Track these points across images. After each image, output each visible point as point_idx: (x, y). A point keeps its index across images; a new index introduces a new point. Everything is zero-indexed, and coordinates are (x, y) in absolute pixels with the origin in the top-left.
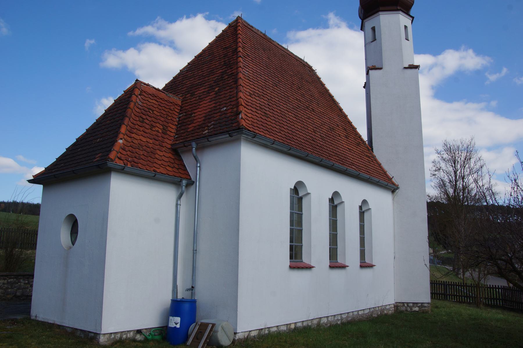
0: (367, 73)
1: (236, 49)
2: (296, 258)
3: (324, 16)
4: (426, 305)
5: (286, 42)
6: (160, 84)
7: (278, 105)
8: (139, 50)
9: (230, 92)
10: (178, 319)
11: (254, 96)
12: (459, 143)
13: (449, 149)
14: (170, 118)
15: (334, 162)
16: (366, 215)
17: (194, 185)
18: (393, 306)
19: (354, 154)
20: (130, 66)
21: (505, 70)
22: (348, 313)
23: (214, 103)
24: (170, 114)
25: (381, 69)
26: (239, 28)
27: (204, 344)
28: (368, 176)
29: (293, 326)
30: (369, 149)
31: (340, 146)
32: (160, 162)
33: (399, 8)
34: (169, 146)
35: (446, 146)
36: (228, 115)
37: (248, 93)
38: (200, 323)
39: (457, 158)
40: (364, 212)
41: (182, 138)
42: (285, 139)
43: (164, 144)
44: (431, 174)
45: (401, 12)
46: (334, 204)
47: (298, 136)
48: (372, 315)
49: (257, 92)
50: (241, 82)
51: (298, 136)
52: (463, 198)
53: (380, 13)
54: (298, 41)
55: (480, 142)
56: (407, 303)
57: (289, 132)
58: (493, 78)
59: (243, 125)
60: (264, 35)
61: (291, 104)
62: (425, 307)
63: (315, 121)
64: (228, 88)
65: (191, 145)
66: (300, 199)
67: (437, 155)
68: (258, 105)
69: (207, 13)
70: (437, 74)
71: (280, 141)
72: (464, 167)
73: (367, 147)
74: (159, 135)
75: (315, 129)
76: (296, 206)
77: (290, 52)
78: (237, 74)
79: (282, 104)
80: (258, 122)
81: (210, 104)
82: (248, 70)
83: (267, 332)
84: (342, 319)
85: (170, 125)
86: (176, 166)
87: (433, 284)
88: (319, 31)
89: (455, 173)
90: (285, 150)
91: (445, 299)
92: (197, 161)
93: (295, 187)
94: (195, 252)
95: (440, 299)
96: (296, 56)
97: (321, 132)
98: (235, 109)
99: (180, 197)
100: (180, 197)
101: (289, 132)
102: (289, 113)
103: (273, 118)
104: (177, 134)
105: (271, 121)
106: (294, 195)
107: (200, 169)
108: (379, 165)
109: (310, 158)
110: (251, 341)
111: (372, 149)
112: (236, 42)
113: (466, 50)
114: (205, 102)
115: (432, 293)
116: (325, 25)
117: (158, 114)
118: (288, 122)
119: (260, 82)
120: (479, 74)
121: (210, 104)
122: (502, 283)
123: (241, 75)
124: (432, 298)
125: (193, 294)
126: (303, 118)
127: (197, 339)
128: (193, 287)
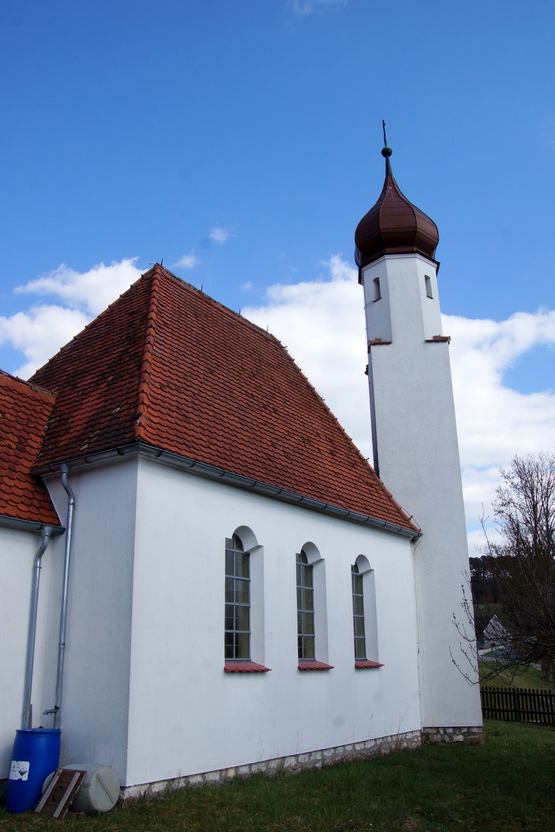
0: (369, 351)
1: (147, 315)
3: (324, 263)
4: (475, 730)
5: (261, 302)
6: (26, 373)
7: (211, 403)
8: (33, 317)
9: (129, 383)
10: (25, 766)
11: (168, 389)
14: (32, 425)
15: (304, 494)
17: (65, 534)
19: (343, 481)
20: (18, 341)
22: (335, 748)
23: (104, 401)
24: (33, 419)
25: (389, 343)
26: (156, 282)
27: (64, 808)
28: (365, 517)
29: (231, 773)
31: (319, 468)
32: (7, 497)
33: (415, 249)
34: (27, 471)
36: (121, 420)
37: (157, 385)
38: (61, 771)
39: (536, 483)
40: (361, 576)
41: (49, 457)
43: (18, 468)
44: (495, 511)
45: (418, 255)
46: (307, 564)
47: (242, 452)
48: (379, 751)
49: (176, 382)
50: (146, 367)
51: (242, 452)
53: (386, 257)
54: (284, 302)
57: (225, 446)
59: (139, 435)
60: (200, 292)
61: (235, 401)
62: (474, 734)
64: (128, 376)
65: (60, 469)
66: (246, 556)
67: (503, 480)
68: (174, 403)
69: (136, 258)
70: (505, 352)
74: (12, 452)
75: (274, 441)
77: (243, 319)
78: (143, 355)
79: (218, 401)
80: (171, 431)
81: (97, 402)
82: (162, 347)
83: (182, 784)
84: (323, 759)
85: (32, 435)
86: (36, 503)
87: (485, 694)
90: (216, 475)
91: (518, 719)
92: (69, 495)
94: (62, 646)
95: (508, 720)
96: (254, 326)
97: (286, 446)
98: (133, 410)
99: (40, 554)
100: (40, 554)
101: (225, 446)
102: (230, 416)
103: (199, 424)
104: (43, 452)
105: (195, 429)
107: (74, 508)
108: (389, 497)
109: (259, 488)
110: (151, 801)
112: (148, 304)
114: (91, 399)
116: (326, 276)
117: (13, 419)
118: (226, 430)
121: (97, 402)
123: (148, 356)
125: (56, 720)
126: (255, 423)
127: (54, 800)
128: (56, 708)
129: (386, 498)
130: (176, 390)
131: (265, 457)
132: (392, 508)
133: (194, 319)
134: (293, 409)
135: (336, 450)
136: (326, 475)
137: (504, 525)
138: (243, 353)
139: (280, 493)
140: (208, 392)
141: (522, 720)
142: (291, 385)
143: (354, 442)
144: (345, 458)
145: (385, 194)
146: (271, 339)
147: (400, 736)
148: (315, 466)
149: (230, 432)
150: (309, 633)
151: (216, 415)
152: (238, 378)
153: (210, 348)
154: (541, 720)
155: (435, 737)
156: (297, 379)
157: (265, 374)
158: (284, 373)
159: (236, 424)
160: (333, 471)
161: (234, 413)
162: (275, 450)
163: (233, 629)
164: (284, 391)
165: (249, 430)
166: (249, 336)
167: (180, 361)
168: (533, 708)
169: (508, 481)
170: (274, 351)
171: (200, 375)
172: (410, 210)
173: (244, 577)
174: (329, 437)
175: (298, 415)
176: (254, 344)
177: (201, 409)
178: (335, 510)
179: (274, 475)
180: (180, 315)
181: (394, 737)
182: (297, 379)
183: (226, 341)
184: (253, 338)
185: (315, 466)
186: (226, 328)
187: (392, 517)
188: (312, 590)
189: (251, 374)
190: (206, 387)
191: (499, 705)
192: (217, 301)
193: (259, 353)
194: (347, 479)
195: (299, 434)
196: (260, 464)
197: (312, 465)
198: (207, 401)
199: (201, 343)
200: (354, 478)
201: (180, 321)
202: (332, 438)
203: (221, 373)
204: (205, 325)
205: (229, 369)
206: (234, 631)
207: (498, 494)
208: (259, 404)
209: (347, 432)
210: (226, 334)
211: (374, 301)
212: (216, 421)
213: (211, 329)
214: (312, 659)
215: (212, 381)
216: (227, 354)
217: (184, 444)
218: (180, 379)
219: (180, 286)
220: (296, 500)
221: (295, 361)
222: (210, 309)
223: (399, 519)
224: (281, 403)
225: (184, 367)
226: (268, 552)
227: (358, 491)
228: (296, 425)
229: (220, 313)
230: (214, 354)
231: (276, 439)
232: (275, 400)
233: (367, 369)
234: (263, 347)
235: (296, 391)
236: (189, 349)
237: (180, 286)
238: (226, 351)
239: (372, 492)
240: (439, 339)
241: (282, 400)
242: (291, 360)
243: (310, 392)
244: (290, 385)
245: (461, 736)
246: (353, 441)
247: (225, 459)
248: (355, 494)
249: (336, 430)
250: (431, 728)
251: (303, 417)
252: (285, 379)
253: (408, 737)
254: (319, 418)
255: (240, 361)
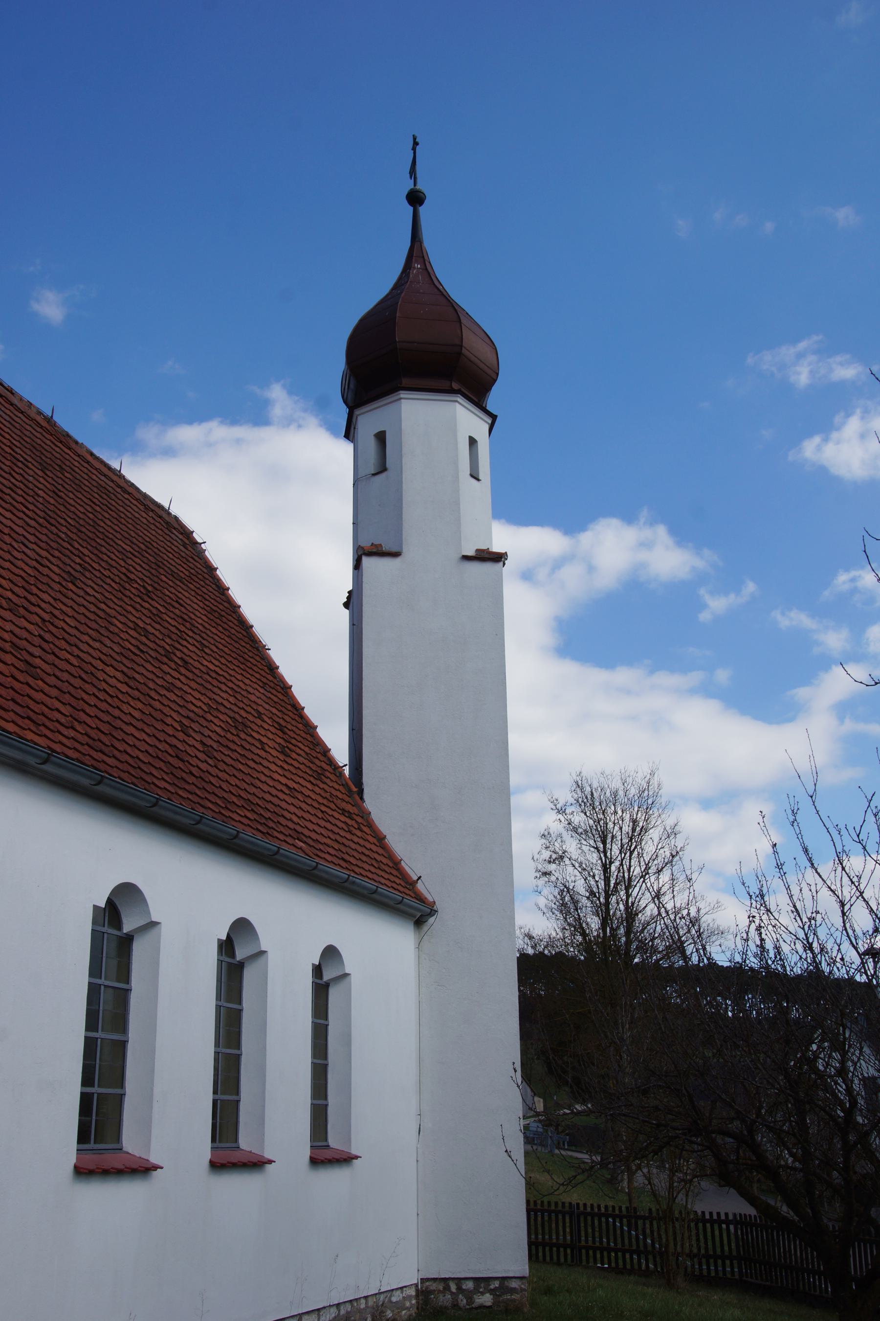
2: (102, 1141)
4: (514, 1284)
5: (137, 449)
7: (73, 640)
12: (616, 784)
13: (588, 801)
16: (334, 995)
18: (413, 1292)
19: (303, 805)
21: (751, 587)
25: (396, 555)
28: (343, 874)
30: (350, 790)
31: (263, 778)
33: (455, 386)
35: (582, 789)
39: (610, 825)
40: (327, 986)
42: (85, 749)
44: (537, 871)
45: (460, 399)
46: (236, 957)
49: (9, 594)
52: (629, 942)
53: (403, 394)
54: (169, 452)
55: (669, 785)
56: (459, 1281)
58: (717, 605)
60: (49, 420)
62: (513, 1291)
63: (189, 698)
66: (126, 943)
67: (554, 816)
71: (70, 753)
72: (631, 853)
73: (345, 785)
76: (109, 964)
79: (86, 638)
88: (239, 431)
89: (606, 868)
90: (85, 782)
93: (110, 902)
95: (558, 1264)
96: (145, 496)
97: (207, 732)
102: (108, 670)
103: (52, 680)
105: (47, 689)
106: (106, 929)
108: (380, 839)
111: (361, 792)
113: (652, 522)
115: (533, 1245)
116: (257, 415)
118: (101, 695)
119: (20, 563)
120: (681, 596)
122: (732, 1205)
124: (533, 1257)
126: (151, 685)
129: (375, 841)
130: (10, 610)
131: (170, 751)
132: (385, 861)
133: (40, 473)
134: (217, 663)
135: (290, 746)
136: (274, 792)
137: (551, 897)
138: (128, 548)
139: (198, 823)
140: (68, 620)
141: (584, 1263)
142: (212, 617)
143: (320, 732)
144: (306, 762)
145: (408, 276)
146: (176, 526)
147: (382, 1297)
148: (255, 775)
149: (109, 700)
150: (231, 1094)
151: (84, 665)
152: (120, 595)
153: (69, 533)
154: (609, 1263)
155: (441, 1297)
156: (221, 607)
157: (167, 593)
158: (200, 593)
159: (119, 685)
160: (286, 785)
161: (114, 663)
162: (186, 739)
163: (94, 1087)
164: (200, 627)
165: (142, 698)
166: (137, 515)
167: (15, 553)
168: (590, 1239)
169: (563, 819)
170: (182, 548)
171: (53, 585)
172: (453, 314)
173: (118, 981)
174: (277, 719)
175: (225, 674)
176: (146, 532)
177: (57, 651)
178: (291, 859)
179: (187, 787)
180: (14, 461)
181: (370, 1299)
182: (221, 607)
183: (99, 522)
184: (145, 521)
185: (255, 775)
186: (96, 495)
187: (386, 876)
188: (241, 1011)
189: (142, 590)
190: (64, 608)
191: (543, 1234)
192: (80, 441)
193: (156, 550)
194: (309, 801)
195: (227, 711)
196: (162, 765)
197: (250, 771)
198: (67, 636)
199: (52, 521)
200: (321, 800)
201: (14, 474)
202: (284, 723)
203: (90, 583)
204: (60, 487)
205: (103, 577)
206: (96, 1089)
207: (544, 841)
208: (158, 649)
209: (307, 712)
210: (98, 509)
211: (374, 475)
212: (84, 676)
213: (71, 495)
214: (234, 1145)
215: (74, 597)
216: (99, 547)
217: (29, 718)
218: (16, 589)
219: (12, 404)
220: (226, 837)
221: (218, 572)
222: (67, 457)
223: (398, 881)
224: (194, 649)
225: (23, 566)
226: (170, 936)
227: (328, 826)
228: (222, 694)
229: (86, 465)
230: (77, 546)
231: (188, 717)
232: (185, 643)
233: (349, 598)
234: (161, 538)
235: (220, 628)
236: (32, 531)
237: (12, 404)
238: (98, 540)
239: (352, 828)
240: (487, 556)
241: (196, 644)
242: (211, 570)
243: (245, 634)
244: (209, 615)
245: (488, 1295)
246: (318, 730)
247: (101, 751)
248: (323, 831)
249: (289, 707)
250: (435, 1279)
251: (233, 679)
252: (201, 604)
253: (394, 1299)
254: (261, 684)
255: (122, 563)
